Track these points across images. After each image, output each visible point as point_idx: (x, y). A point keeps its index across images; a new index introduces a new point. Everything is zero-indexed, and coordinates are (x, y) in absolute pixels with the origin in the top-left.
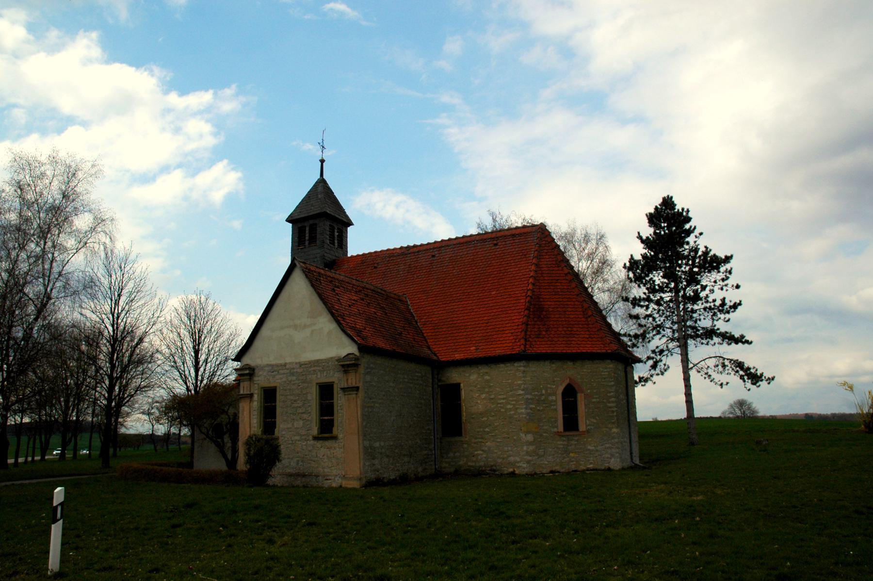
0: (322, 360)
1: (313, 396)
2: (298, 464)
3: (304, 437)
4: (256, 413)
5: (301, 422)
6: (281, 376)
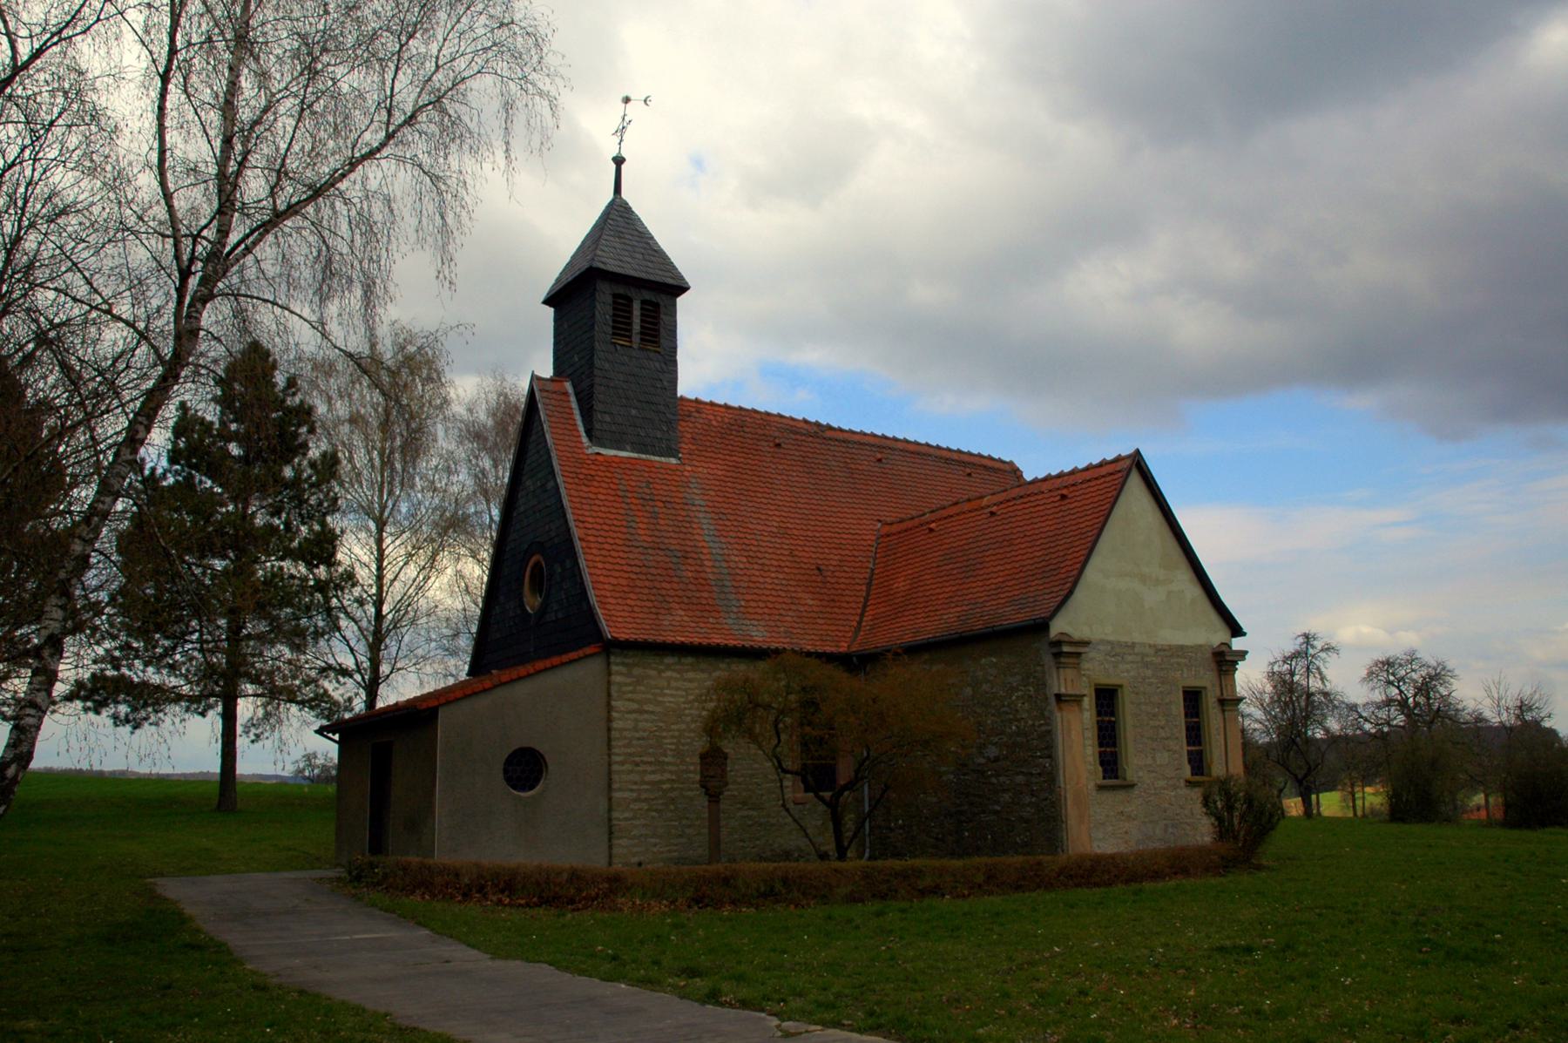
0: (1187, 646)
1: (1178, 708)
2: (1166, 831)
3: (1171, 782)
4: (1090, 735)
5: (1166, 754)
6: (1128, 666)
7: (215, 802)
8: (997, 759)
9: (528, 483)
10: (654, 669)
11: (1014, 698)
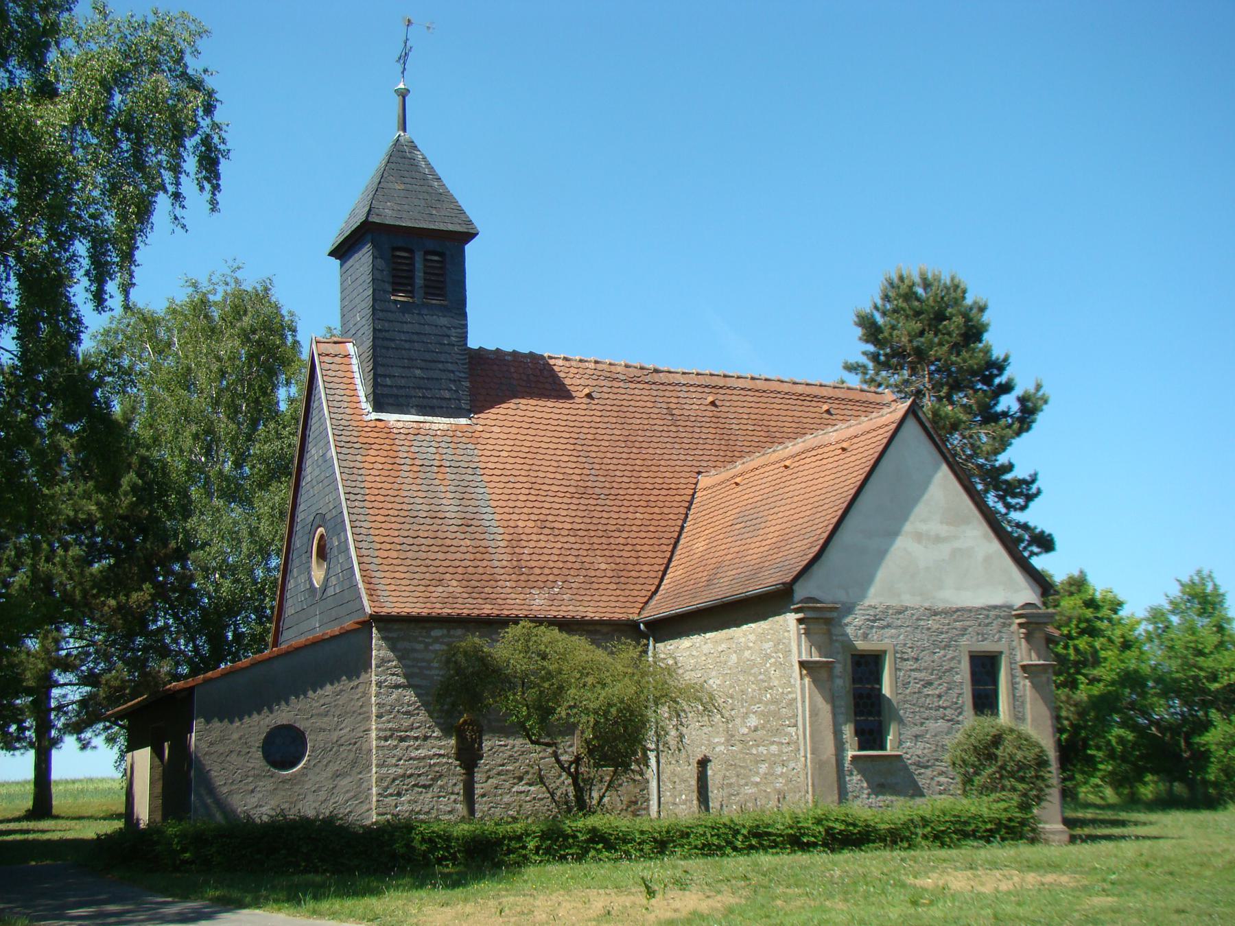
4: (843, 703)
7: (29, 804)
8: (756, 729)
9: (313, 451)
10: (420, 642)
11: (768, 665)
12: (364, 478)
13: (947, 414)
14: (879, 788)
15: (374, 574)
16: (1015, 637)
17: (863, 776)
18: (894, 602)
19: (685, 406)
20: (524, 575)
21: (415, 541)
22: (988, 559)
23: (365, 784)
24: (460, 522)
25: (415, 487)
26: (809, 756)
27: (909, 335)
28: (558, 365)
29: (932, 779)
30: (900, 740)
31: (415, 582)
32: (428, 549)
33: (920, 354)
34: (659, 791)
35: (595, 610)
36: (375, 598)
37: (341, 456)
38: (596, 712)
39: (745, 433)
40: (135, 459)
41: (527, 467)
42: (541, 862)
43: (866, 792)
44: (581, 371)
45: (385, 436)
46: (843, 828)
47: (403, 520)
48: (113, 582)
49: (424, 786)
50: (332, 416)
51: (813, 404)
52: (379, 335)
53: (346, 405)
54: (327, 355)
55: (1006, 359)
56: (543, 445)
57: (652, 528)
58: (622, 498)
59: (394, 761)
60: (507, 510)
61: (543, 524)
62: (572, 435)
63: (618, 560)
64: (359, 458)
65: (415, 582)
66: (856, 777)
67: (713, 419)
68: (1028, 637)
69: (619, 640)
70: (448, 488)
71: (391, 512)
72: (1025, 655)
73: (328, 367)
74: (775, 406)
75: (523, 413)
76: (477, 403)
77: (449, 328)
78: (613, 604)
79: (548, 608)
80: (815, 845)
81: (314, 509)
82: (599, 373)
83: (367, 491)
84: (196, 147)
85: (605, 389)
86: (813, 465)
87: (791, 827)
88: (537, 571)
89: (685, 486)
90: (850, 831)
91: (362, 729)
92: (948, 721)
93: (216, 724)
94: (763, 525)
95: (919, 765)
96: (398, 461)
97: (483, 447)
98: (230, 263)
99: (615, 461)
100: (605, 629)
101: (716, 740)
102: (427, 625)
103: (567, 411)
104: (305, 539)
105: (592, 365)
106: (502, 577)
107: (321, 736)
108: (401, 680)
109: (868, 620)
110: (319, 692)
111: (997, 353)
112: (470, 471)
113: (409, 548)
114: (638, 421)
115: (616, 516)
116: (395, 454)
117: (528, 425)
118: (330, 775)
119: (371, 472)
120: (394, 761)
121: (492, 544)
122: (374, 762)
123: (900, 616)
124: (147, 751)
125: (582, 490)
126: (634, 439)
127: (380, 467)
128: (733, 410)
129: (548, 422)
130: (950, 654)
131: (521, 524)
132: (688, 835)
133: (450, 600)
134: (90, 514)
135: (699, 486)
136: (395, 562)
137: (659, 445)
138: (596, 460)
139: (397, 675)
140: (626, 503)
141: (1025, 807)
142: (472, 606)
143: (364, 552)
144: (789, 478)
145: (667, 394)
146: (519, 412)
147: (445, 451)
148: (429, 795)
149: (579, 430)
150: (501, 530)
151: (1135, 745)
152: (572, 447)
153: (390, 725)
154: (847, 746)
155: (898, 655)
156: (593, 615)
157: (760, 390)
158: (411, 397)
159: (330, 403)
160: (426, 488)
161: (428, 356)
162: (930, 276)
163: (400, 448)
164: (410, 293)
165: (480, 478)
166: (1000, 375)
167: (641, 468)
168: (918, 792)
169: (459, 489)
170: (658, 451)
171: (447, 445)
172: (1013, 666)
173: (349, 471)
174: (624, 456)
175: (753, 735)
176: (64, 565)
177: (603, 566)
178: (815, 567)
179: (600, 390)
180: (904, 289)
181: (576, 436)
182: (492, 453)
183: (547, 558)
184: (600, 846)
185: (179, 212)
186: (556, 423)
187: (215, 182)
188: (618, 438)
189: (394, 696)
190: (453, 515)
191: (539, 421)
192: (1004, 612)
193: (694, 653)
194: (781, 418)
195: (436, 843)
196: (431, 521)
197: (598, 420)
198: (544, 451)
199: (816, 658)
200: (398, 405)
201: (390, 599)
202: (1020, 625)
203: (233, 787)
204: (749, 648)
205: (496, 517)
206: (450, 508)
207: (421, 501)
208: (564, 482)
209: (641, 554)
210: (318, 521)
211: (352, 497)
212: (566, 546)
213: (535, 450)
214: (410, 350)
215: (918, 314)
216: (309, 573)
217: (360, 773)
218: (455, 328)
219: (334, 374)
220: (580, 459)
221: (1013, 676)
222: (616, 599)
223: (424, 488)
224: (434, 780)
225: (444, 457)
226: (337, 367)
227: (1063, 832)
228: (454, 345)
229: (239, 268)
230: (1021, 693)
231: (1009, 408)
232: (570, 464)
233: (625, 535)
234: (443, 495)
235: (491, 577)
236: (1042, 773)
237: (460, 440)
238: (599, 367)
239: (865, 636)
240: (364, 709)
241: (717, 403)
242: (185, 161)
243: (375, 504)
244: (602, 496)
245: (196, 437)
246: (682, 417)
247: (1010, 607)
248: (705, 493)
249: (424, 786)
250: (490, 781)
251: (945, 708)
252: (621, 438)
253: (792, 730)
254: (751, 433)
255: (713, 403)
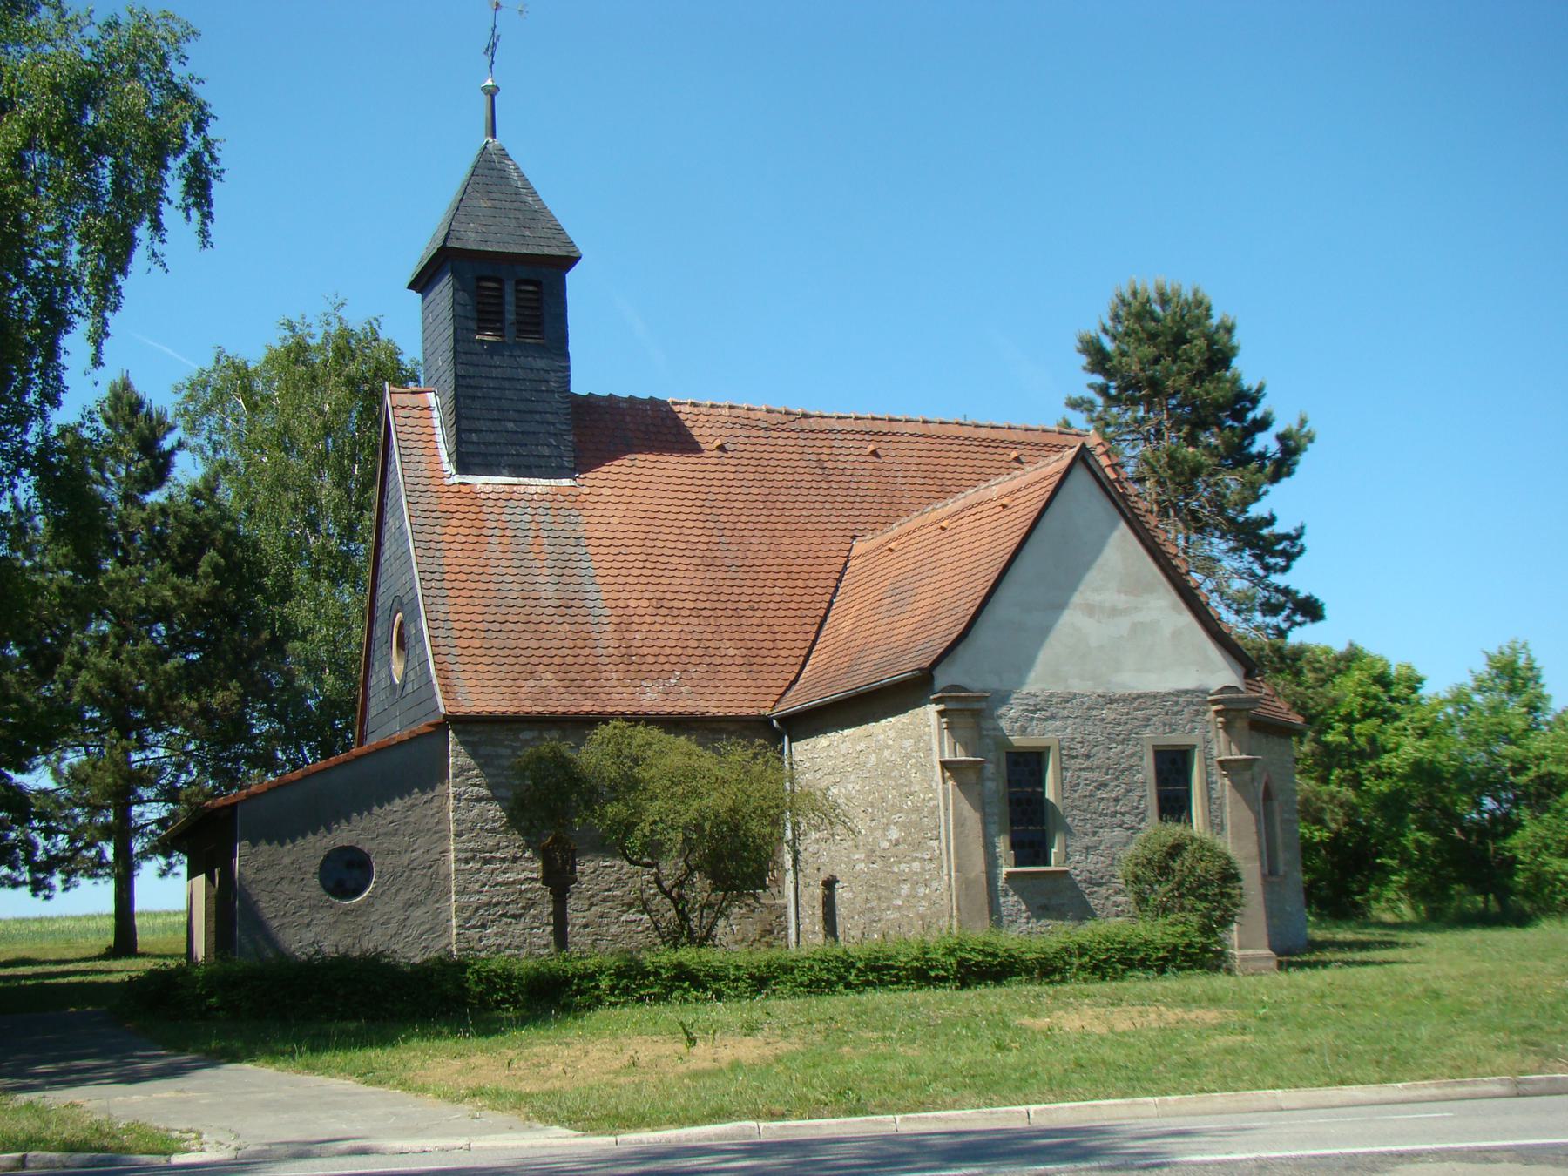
7: (110, 939)
9: (391, 523)
10: (506, 747)
12: (443, 553)
13: (1185, 457)
14: (1041, 910)
15: (451, 667)
16: (1211, 727)
17: (1021, 896)
18: (1059, 689)
19: (840, 458)
20: (633, 665)
21: (503, 627)
22: (1177, 635)
23: (443, 915)
24: (558, 603)
25: (504, 563)
26: (953, 874)
27: (1140, 362)
28: (684, 412)
29: (1107, 898)
30: (1067, 853)
31: (501, 675)
32: (518, 635)
33: (1155, 385)
34: (797, 918)
35: (719, 704)
36: (452, 695)
37: (416, 528)
38: (686, 827)
39: (913, 488)
40: (218, 535)
41: (642, 536)
42: (617, 1004)
43: (1024, 915)
44: (712, 418)
45: (471, 502)
46: (980, 958)
47: (489, 602)
48: (194, 679)
49: (514, 916)
50: (407, 480)
51: (1000, 451)
52: (463, 382)
53: (424, 466)
54: (403, 408)
55: (1260, 390)
56: (663, 508)
57: (792, 605)
58: (758, 569)
59: (477, 887)
60: (615, 587)
61: (659, 604)
62: (699, 496)
63: (750, 644)
64: (438, 529)
65: (501, 675)
66: (1013, 899)
67: (874, 472)
68: (1227, 727)
69: (728, 739)
70: (545, 563)
71: (475, 593)
72: (1222, 748)
73: (403, 421)
74: (951, 454)
75: (639, 471)
76: (584, 459)
77: (547, 372)
78: (743, 697)
79: (662, 703)
80: (944, 979)
81: (392, 590)
82: (735, 421)
83: (447, 569)
84: (184, 167)
85: (741, 440)
86: (971, 525)
87: (917, 960)
88: (651, 659)
89: (835, 554)
90: (989, 963)
91: (439, 850)
92: (1127, 829)
93: (263, 847)
94: (912, 599)
95: (1090, 882)
96: (485, 532)
97: (589, 513)
98: (332, 299)
99: (750, 526)
100: (732, 727)
101: (857, 857)
102: (517, 726)
103: (694, 468)
104: (385, 627)
105: (726, 411)
106: (607, 668)
107: (390, 859)
108: (484, 792)
109: (1027, 710)
110: (387, 807)
111: (1249, 382)
112: (572, 542)
113: (495, 635)
114: (781, 477)
115: (750, 591)
116: (482, 524)
117: (646, 486)
118: (401, 905)
119: (452, 546)
120: (477, 887)
121: (596, 628)
122: (453, 889)
123: (1068, 705)
124: (202, 877)
125: (710, 561)
126: (775, 498)
127: (464, 539)
128: (898, 460)
129: (669, 480)
130: (1130, 749)
131: (632, 603)
132: (792, 969)
133: (543, 696)
134: (164, 601)
135: (852, 554)
136: (477, 652)
137: (806, 505)
138: (727, 526)
139: (479, 786)
140: (762, 576)
141: (1206, 930)
142: (569, 703)
143: (441, 641)
144: (945, 541)
145: (818, 443)
146: (634, 470)
147: (542, 518)
148: (521, 926)
149: (707, 490)
150: (608, 612)
151: (1436, 851)
152: (698, 510)
153: (472, 845)
154: (1001, 861)
155: (1065, 752)
156: (715, 710)
157: (934, 436)
158: (502, 455)
159: (405, 465)
160: (518, 563)
161: (521, 406)
162: (1168, 290)
163: (488, 516)
164: (499, 331)
165: (584, 550)
166: (1253, 408)
167: (782, 533)
168: (1084, 912)
169: (559, 564)
170: (804, 512)
171: (545, 512)
172: (1209, 762)
173: (426, 546)
174: (763, 519)
175: (894, 850)
176: (133, 663)
177: (731, 652)
178: (960, 648)
179: (736, 440)
180: (1135, 306)
181: (704, 497)
182: (601, 519)
183: (662, 643)
184: (687, 984)
185: (157, 246)
186: (679, 481)
187: (206, 209)
188: (755, 498)
189: (476, 811)
190: (550, 595)
191: (659, 480)
192: (1198, 698)
193: (832, 754)
194: (959, 469)
195: (495, 983)
196: (522, 603)
197: (732, 476)
198: (664, 516)
199: (962, 757)
200: (487, 466)
201: (469, 696)
202: (1217, 712)
203: (286, 920)
204: (889, 747)
205: (603, 596)
206: (546, 586)
207: (511, 579)
208: (687, 553)
209: (778, 636)
210: (396, 606)
211: (428, 576)
212: (686, 628)
213: (653, 515)
214: (500, 399)
215: (1152, 337)
216: (390, 667)
217: (437, 902)
218: (555, 371)
219: (411, 430)
220: (708, 525)
221: (1208, 774)
222: (746, 690)
223: (516, 563)
224: (526, 908)
225: (542, 525)
226: (415, 422)
227: (1268, 958)
228: (553, 392)
229: (343, 304)
230: (1219, 794)
231: (1266, 448)
232: (695, 531)
233: (759, 613)
234: (538, 571)
235: (593, 668)
236: (1228, 890)
237: (561, 505)
238: (735, 412)
239: (1023, 730)
240: (440, 827)
241: (880, 452)
242: (167, 186)
243: (456, 584)
244: (733, 568)
245: (295, 507)
246: (835, 471)
247: (1205, 692)
248: (859, 561)
249: (514, 916)
250: (593, 909)
251: (1123, 814)
252: (759, 498)
253: (934, 843)
254: (920, 488)
255: (874, 453)
